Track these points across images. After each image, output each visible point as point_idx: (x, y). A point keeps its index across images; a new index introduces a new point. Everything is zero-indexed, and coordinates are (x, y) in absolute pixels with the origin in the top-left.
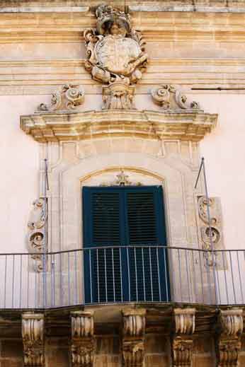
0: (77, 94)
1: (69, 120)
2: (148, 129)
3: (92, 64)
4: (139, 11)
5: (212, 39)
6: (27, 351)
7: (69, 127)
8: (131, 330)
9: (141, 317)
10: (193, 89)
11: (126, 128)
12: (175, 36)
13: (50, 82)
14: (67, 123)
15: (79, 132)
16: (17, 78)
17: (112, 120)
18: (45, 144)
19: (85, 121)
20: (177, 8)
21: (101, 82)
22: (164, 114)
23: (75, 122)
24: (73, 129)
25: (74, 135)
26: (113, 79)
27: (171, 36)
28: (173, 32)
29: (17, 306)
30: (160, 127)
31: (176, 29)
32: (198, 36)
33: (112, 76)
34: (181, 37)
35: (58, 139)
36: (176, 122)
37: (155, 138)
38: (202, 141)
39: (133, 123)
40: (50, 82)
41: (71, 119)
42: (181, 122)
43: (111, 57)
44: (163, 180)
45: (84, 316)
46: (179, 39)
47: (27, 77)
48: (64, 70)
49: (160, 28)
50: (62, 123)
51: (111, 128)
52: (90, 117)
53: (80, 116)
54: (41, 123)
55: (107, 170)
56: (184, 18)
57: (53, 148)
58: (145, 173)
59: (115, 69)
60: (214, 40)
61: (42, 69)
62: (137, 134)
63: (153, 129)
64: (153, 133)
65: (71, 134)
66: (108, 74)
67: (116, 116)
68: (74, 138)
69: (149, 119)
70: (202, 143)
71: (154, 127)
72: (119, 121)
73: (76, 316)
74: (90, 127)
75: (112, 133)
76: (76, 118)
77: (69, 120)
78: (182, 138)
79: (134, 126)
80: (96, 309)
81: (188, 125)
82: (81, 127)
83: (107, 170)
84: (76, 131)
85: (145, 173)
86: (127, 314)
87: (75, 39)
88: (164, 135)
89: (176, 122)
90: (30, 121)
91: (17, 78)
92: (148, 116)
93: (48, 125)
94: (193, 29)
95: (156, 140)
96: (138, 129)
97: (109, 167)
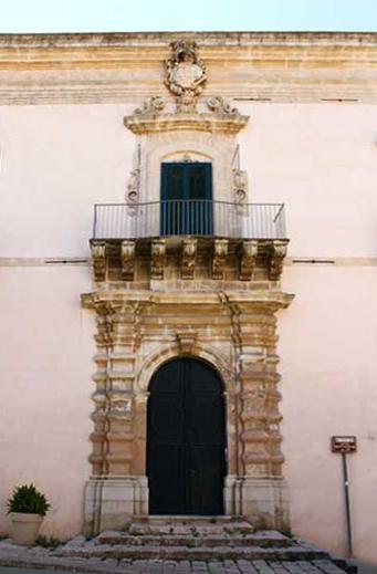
28: (223, 61)
49: (216, 58)
54: (137, 121)
55: (178, 152)
70: (238, 135)
83: (178, 152)
97: (178, 150)
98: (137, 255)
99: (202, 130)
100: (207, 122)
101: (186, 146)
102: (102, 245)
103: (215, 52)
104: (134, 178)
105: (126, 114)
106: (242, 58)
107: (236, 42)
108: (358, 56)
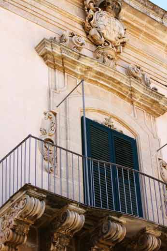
0: (81, 42)
1: (78, 59)
2: (127, 93)
3: (91, 26)
4: (128, 4)
5: (162, 49)
6: (57, 239)
7: (76, 64)
8: (150, 246)
9: (158, 238)
10: (151, 78)
11: (112, 85)
12: (141, 35)
13: (58, 25)
14: (77, 60)
15: (81, 72)
16: (33, 8)
17: (106, 73)
18: (53, 70)
19: (89, 65)
20: (152, 16)
21: (95, 44)
22: (143, 87)
23: (83, 63)
24: (79, 67)
25: (77, 72)
26: (106, 44)
27: (137, 33)
28: (141, 31)
29: (64, 195)
30: (136, 95)
31: (144, 30)
32: (155, 43)
33: (105, 41)
34: (145, 37)
35: (64, 70)
36: (149, 96)
37: (129, 102)
38: (159, 118)
39: (119, 83)
40: (58, 25)
41: (81, 59)
42: (152, 98)
43: (107, 28)
44: (136, 135)
45: (118, 222)
46: (143, 38)
47: (41, 12)
48: (68, 21)
49: (135, 25)
50: (74, 59)
51: (103, 80)
52: (93, 64)
53: (87, 59)
54: (57, 51)
55: (99, 111)
56: (153, 25)
57: (59, 75)
58: (124, 125)
59: (108, 37)
60: (163, 51)
61: (53, 13)
62: (119, 93)
63: (131, 95)
64: (130, 98)
65: (75, 71)
66: (103, 39)
67: (110, 73)
68: (76, 75)
69: (132, 86)
70: (158, 119)
71: (132, 93)
72: (110, 77)
73: (113, 220)
74: (89, 72)
75: (102, 84)
76: (83, 60)
77: (78, 59)
78: (148, 109)
79: (118, 85)
80: (128, 220)
81: (155, 102)
82: (84, 69)
83: (99, 111)
84: (79, 70)
85: (124, 125)
86: (148, 232)
87: (78, 4)
88: (137, 102)
89: (149, 96)
90: (50, 46)
91: (33, 8)
92: (132, 83)
93: (62, 55)
94: (155, 36)
95: (129, 104)
96: (121, 89)
97: (101, 109)
98: (76, 236)
99: (123, 97)
100: (132, 90)
101: (110, 108)
102: (41, 199)
103: (135, 18)
104: (48, 121)
105: (46, 37)
106: (158, 38)
107: (159, 19)
108: (63, 116)
